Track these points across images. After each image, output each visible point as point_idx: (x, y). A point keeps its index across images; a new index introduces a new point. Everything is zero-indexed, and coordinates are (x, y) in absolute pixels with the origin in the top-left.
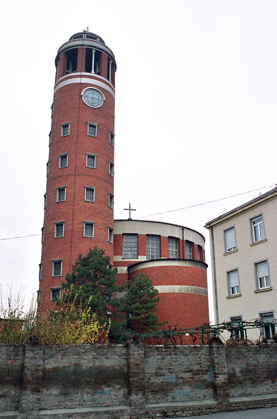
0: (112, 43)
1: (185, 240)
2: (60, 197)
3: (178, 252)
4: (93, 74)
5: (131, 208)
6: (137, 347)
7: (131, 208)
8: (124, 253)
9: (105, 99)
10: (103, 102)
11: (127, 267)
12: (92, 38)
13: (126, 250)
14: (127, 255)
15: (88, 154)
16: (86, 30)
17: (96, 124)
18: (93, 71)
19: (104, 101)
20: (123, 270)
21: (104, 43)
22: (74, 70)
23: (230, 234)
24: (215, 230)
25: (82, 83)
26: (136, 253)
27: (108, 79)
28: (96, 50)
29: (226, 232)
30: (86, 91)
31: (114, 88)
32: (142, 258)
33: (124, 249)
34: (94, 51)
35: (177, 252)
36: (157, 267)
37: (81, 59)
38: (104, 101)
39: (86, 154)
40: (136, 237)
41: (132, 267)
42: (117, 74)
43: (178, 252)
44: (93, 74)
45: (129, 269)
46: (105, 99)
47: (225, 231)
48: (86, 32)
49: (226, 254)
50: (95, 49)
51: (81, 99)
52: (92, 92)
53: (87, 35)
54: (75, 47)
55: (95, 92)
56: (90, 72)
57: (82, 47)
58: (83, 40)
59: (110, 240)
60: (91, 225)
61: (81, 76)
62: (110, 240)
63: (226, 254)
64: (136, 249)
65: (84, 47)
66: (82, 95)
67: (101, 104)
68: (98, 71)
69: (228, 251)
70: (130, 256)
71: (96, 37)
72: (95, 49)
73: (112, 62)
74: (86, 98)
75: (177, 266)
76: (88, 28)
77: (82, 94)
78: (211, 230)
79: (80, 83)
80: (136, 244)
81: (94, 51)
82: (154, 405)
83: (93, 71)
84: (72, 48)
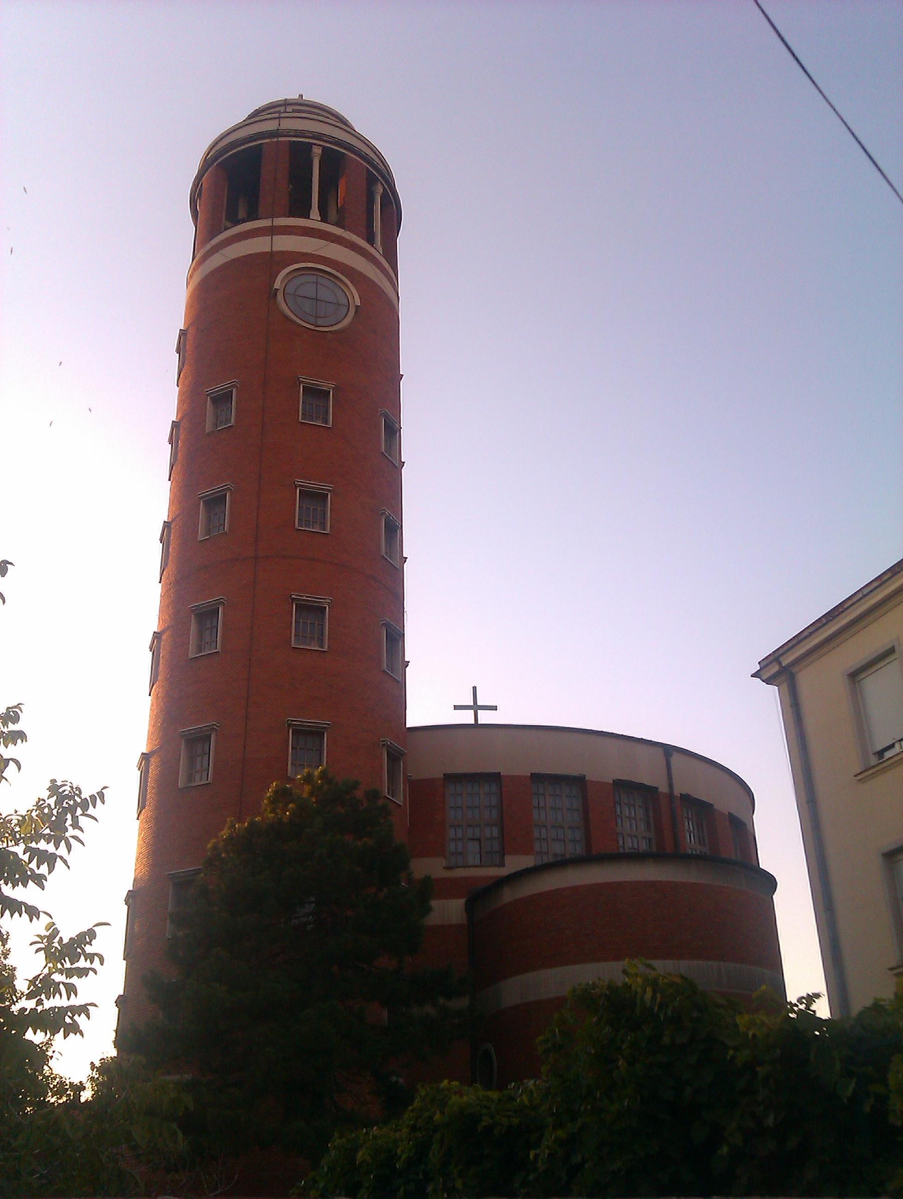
0: (377, 122)
1: (677, 792)
2: (201, 640)
3: (654, 842)
4: (314, 220)
5: (472, 711)
7: (472, 711)
8: (452, 847)
9: (358, 303)
10: (352, 311)
11: (463, 901)
12: (310, 113)
13: (460, 835)
14: (461, 853)
15: (300, 486)
17: (326, 385)
18: (315, 213)
20: (449, 911)
22: (253, 215)
23: (880, 687)
24: (807, 679)
25: (277, 252)
26: (496, 846)
27: (371, 240)
28: (324, 148)
29: (857, 679)
30: (295, 275)
31: (394, 279)
32: (515, 863)
33: (451, 833)
34: (317, 151)
35: (650, 840)
36: (576, 889)
37: (274, 177)
40: (494, 788)
41: (479, 896)
42: (402, 241)
43: (654, 842)
44: (314, 220)
45: (470, 907)
46: (358, 303)
47: (855, 676)
49: (866, 774)
50: (321, 143)
52: (314, 279)
54: (249, 142)
55: (322, 281)
57: (275, 140)
58: (279, 118)
59: (392, 791)
60: (317, 734)
61: (273, 231)
62: (392, 791)
63: (866, 774)
64: (495, 832)
66: (277, 290)
68: (333, 215)
69: (874, 761)
70: (474, 859)
72: (321, 143)
73: (384, 189)
75: (653, 884)
77: (277, 285)
78: (785, 686)
79: (271, 254)
80: (495, 813)
81: (317, 151)
82: (472, 869)
83: (315, 213)
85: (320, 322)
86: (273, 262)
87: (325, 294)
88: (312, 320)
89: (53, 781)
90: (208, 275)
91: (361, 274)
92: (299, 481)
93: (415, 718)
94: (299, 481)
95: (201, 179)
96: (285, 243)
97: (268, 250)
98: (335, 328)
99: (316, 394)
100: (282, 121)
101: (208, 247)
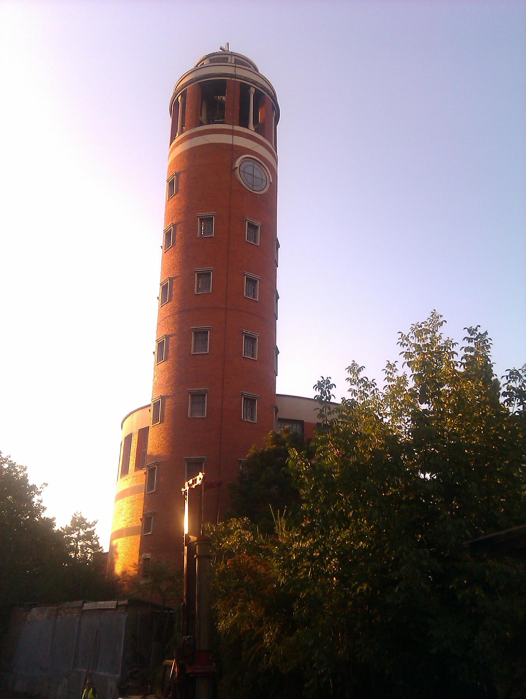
0: (272, 69)
6: (143, 433)
10: (268, 185)
16: (224, 46)
19: (271, 183)
21: (256, 69)
28: (256, 88)
34: (253, 90)
38: (271, 183)
39: (245, 275)
44: (251, 130)
48: (226, 53)
50: (255, 86)
51: (234, 174)
52: (251, 163)
53: (235, 59)
55: (255, 165)
56: (247, 127)
61: (233, 133)
65: (236, 80)
67: (266, 189)
71: (226, 56)
74: (242, 173)
76: (228, 44)
77: (237, 164)
81: (253, 90)
84: (206, 80)
85: (255, 188)
86: (235, 151)
87: (257, 174)
88: (251, 187)
89: (354, 364)
90: (195, 147)
91: (203, 131)
92: (246, 273)
93: (280, 389)
94: (246, 273)
95: (187, 86)
96: (240, 141)
97: (230, 143)
98: (262, 192)
99: (252, 226)
100: (237, 69)
101: (194, 130)
